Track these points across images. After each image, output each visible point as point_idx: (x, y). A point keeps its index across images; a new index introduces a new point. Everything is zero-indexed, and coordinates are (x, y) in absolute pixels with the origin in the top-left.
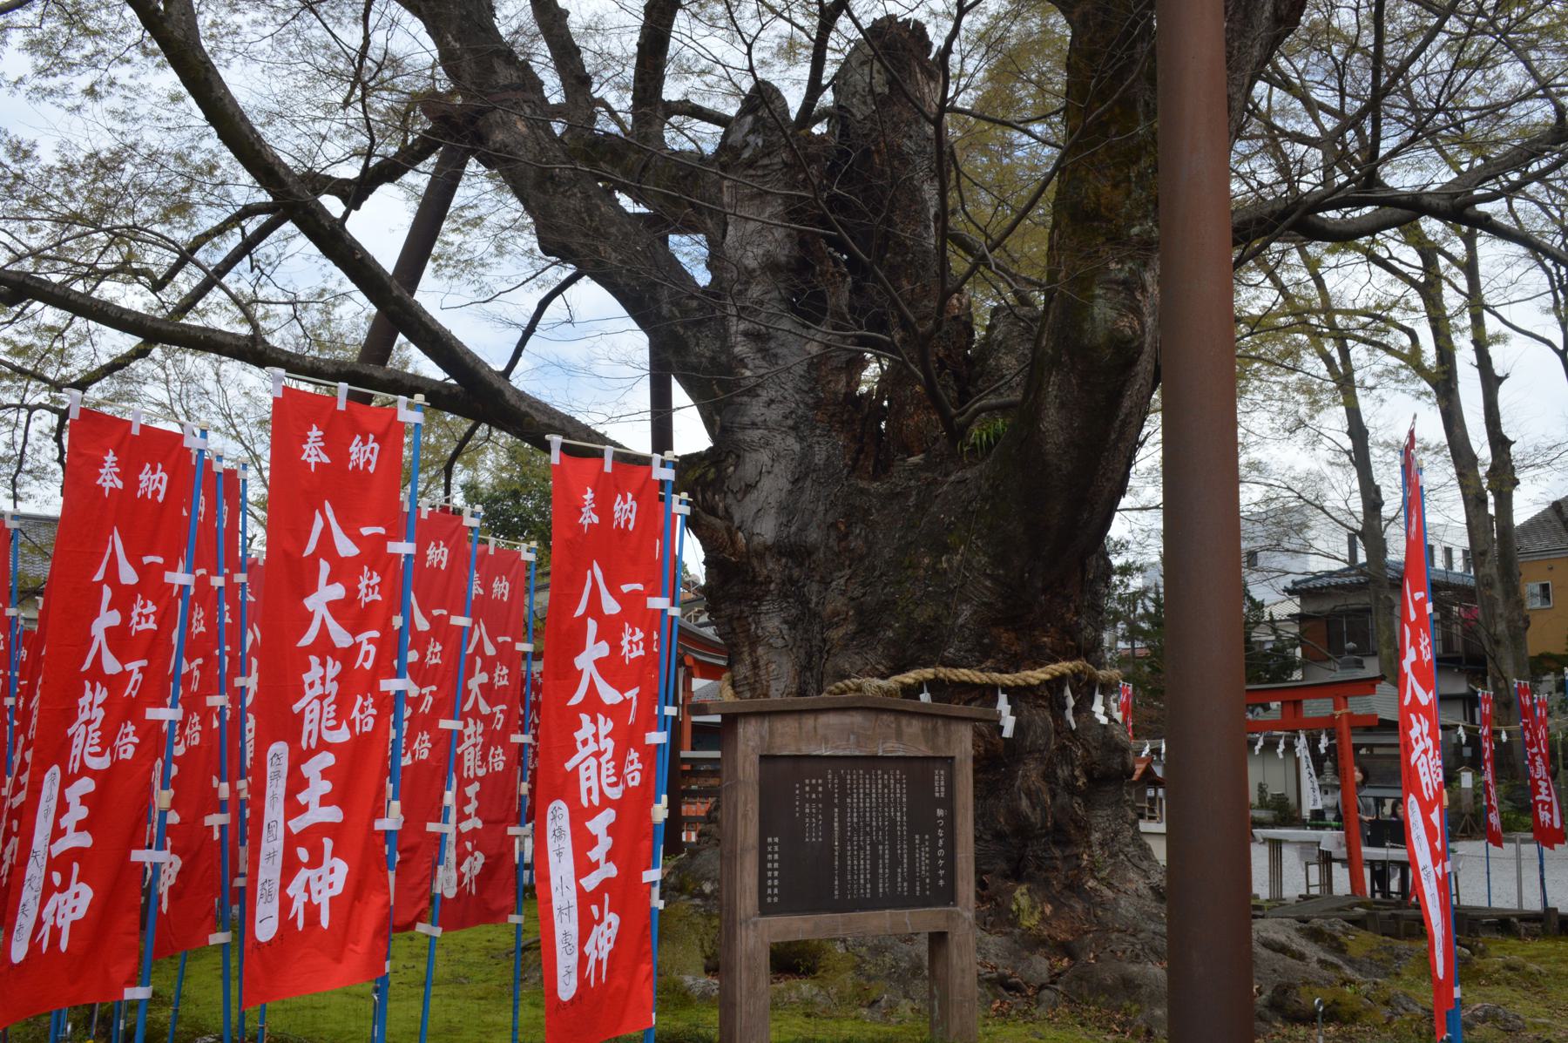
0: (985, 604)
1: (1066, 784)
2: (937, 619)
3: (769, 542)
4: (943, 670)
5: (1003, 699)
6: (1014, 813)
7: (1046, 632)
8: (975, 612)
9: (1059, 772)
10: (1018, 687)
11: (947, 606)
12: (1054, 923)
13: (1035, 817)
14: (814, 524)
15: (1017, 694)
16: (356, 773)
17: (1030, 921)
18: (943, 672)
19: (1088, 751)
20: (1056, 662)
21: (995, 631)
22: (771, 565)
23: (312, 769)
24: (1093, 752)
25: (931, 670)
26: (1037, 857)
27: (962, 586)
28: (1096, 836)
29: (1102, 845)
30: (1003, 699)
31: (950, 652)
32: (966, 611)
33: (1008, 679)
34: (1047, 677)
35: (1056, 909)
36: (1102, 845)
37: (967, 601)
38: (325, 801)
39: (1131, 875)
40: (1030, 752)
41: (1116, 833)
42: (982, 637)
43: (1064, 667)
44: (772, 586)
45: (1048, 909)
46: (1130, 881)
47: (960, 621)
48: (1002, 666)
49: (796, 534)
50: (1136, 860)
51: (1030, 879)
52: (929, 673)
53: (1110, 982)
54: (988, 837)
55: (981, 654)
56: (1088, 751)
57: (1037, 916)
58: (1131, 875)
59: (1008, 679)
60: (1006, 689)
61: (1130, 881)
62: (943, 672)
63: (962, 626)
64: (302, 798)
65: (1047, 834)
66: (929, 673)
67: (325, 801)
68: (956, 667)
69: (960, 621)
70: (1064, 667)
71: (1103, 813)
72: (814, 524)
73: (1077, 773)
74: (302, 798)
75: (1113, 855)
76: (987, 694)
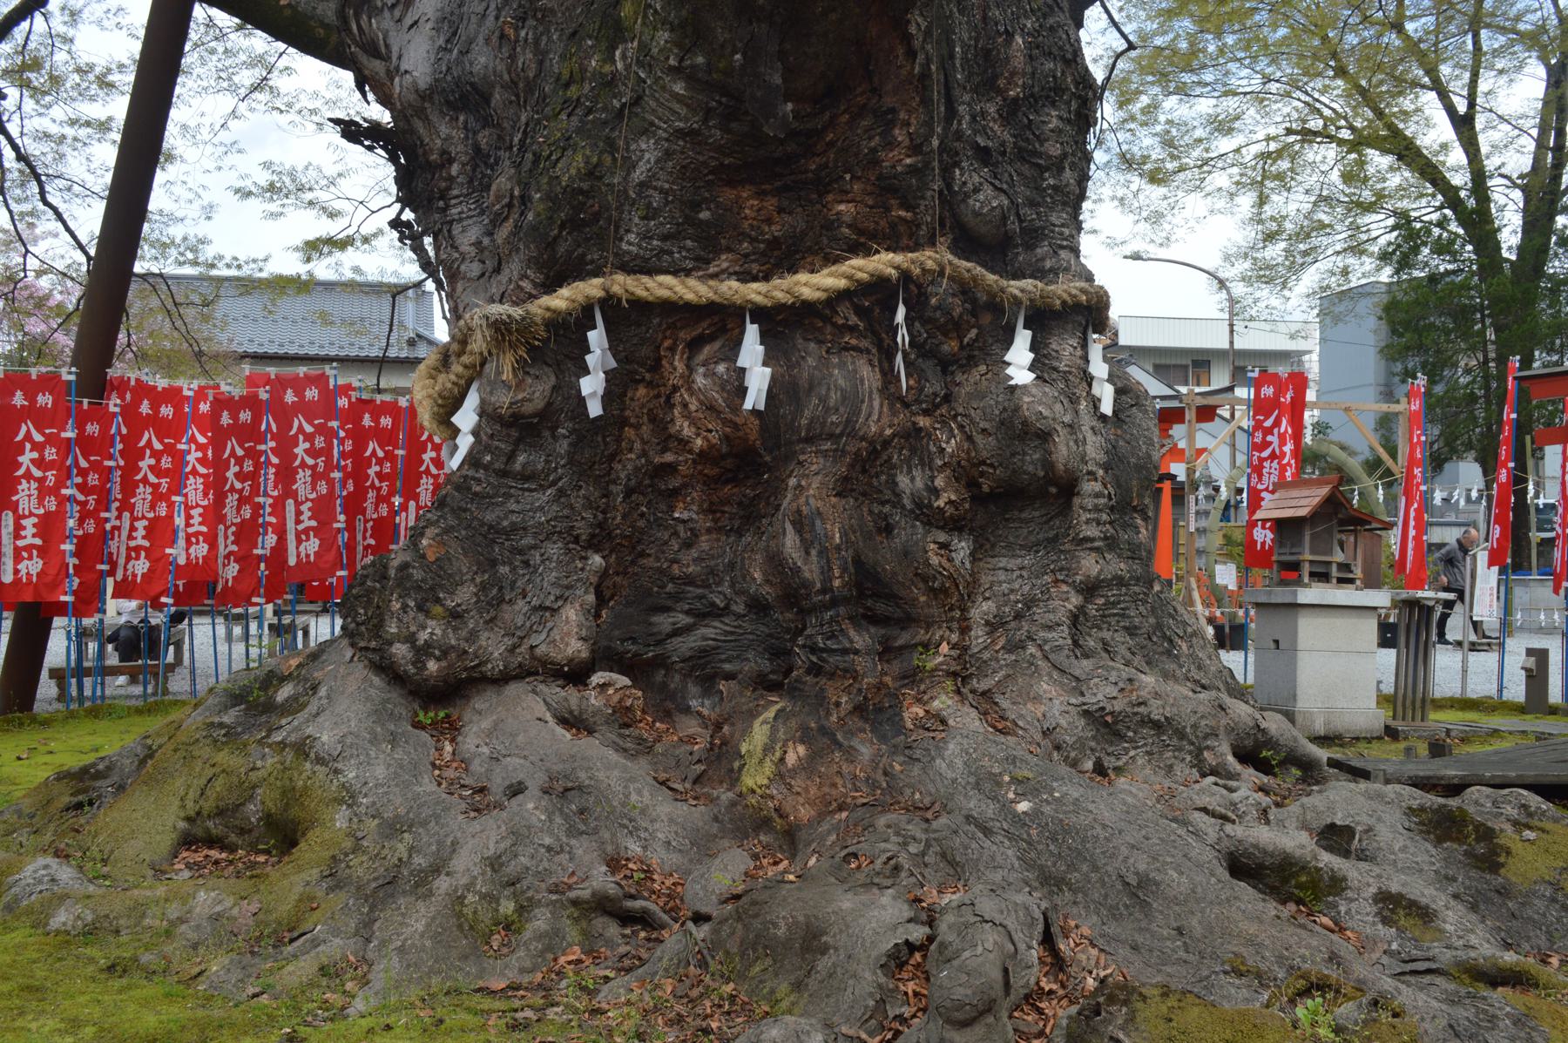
0: (680, 134)
1: (919, 504)
2: (592, 173)
3: (422, 85)
4: (620, 278)
5: (752, 332)
6: (776, 561)
7: (844, 197)
8: (668, 154)
9: (903, 481)
10: (780, 307)
11: (611, 146)
12: (798, 783)
13: (811, 570)
14: (481, 40)
15: (782, 324)
16: (322, 509)
17: (755, 778)
18: (622, 284)
19: (969, 438)
20: (868, 253)
21: (728, 195)
22: (444, 130)
23: (304, 508)
24: (979, 439)
25: (597, 281)
26: (814, 649)
27: (637, 101)
28: (982, 609)
29: (993, 626)
30: (752, 332)
31: (630, 243)
32: (647, 153)
33: (754, 292)
34: (842, 283)
35: (814, 757)
36: (993, 626)
37: (646, 131)
38: (34, 536)
39: (1045, 687)
40: (809, 440)
41: (1030, 602)
42: (696, 206)
43: (884, 262)
44: (455, 169)
45: (796, 754)
46: (1037, 699)
47: (639, 174)
48: (755, 268)
49: (458, 62)
50: (1060, 658)
51: (793, 692)
52: (592, 288)
53: (781, 932)
54: (739, 608)
55: (704, 245)
56: (969, 438)
57: (769, 768)
58: (1045, 687)
59: (754, 292)
60: (761, 314)
61: (1037, 699)
62: (622, 284)
63: (642, 184)
64: (23, 533)
65: (834, 603)
66: (592, 288)
67: (34, 536)
68: (650, 272)
69: (639, 174)
70: (884, 262)
71: (1013, 563)
72: (481, 40)
73: (939, 482)
74: (23, 533)
75: (1015, 647)
76: (722, 323)
